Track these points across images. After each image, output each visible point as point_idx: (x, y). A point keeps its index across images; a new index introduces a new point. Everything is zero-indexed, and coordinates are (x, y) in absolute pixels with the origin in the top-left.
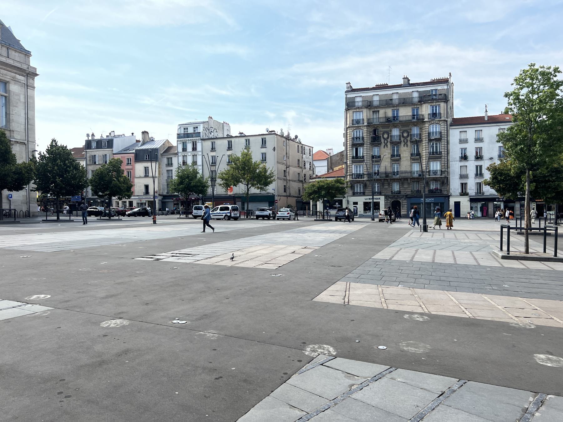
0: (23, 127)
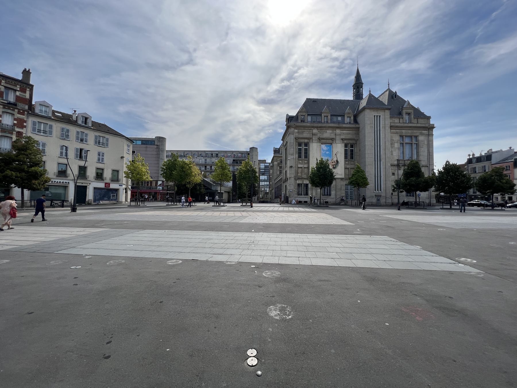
0: (426, 157)
